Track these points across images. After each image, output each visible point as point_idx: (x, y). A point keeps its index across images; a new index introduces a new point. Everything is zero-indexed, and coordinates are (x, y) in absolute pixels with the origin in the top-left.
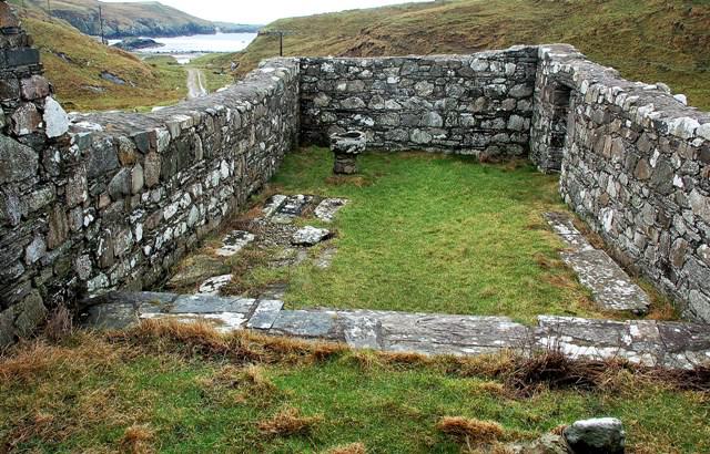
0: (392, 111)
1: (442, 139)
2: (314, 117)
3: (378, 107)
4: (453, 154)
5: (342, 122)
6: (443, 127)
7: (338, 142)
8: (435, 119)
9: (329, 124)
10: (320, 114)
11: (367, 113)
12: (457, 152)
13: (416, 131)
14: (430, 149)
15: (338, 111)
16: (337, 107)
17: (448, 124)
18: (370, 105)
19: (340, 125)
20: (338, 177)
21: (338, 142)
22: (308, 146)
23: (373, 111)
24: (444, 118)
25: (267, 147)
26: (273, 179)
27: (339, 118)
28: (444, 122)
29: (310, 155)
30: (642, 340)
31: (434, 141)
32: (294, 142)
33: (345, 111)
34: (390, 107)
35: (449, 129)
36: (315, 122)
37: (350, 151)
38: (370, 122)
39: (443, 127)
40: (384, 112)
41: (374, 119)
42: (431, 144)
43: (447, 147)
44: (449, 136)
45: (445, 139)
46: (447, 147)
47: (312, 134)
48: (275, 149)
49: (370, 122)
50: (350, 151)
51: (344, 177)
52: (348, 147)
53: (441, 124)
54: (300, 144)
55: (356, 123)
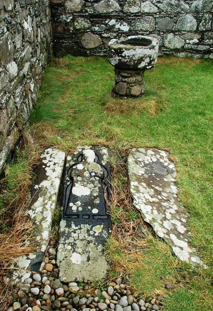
0: (148, 14)
1: (194, 44)
2: (67, 24)
3: (134, 10)
4: (202, 58)
5: (97, 29)
6: (197, 31)
7: (126, 53)
8: (190, 22)
9: (83, 31)
10: (73, 20)
11: (122, 17)
12: (206, 56)
13: (170, 36)
14: (182, 55)
15: (91, 16)
16: (90, 11)
17: (202, 28)
18: (126, 8)
19: (94, 32)
20: (124, 101)
21: (126, 53)
22: (63, 56)
23: (129, 14)
24: (199, 20)
25: (20, 66)
26: (36, 116)
27: (93, 23)
28: (198, 26)
29: (68, 66)
30: (31, 187)
31: (186, 46)
32: (49, 53)
33: (99, 16)
34: (146, 10)
35: (202, 33)
36: (69, 30)
37: (142, 65)
38: (125, 28)
39: (197, 31)
40: (139, 15)
41: (129, 24)
42: (183, 49)
43: (198, 52)
44: (201, 41)
45: (197, 44)
46: (198, 52)
47: (67, 43)
48: (32, 67)
49: (125, 28)
50: (142, 65)
51: (132, 102)
52: (141, 60)
53: (195, 29)
54: (55, 55)
55: (110, 29)
